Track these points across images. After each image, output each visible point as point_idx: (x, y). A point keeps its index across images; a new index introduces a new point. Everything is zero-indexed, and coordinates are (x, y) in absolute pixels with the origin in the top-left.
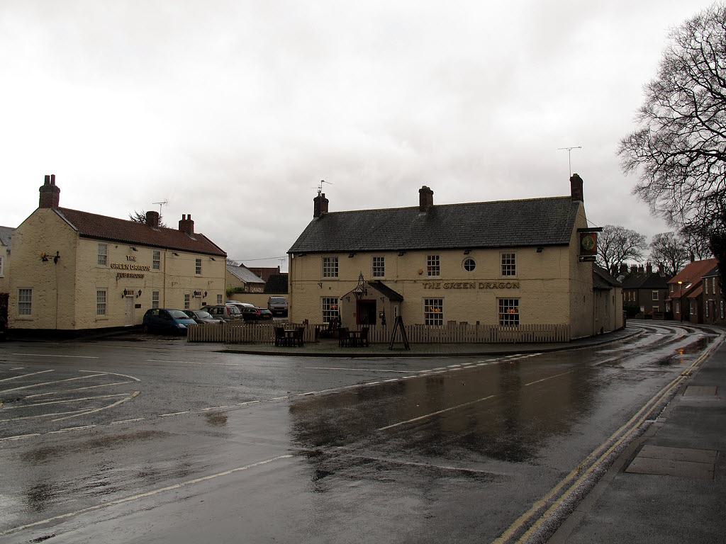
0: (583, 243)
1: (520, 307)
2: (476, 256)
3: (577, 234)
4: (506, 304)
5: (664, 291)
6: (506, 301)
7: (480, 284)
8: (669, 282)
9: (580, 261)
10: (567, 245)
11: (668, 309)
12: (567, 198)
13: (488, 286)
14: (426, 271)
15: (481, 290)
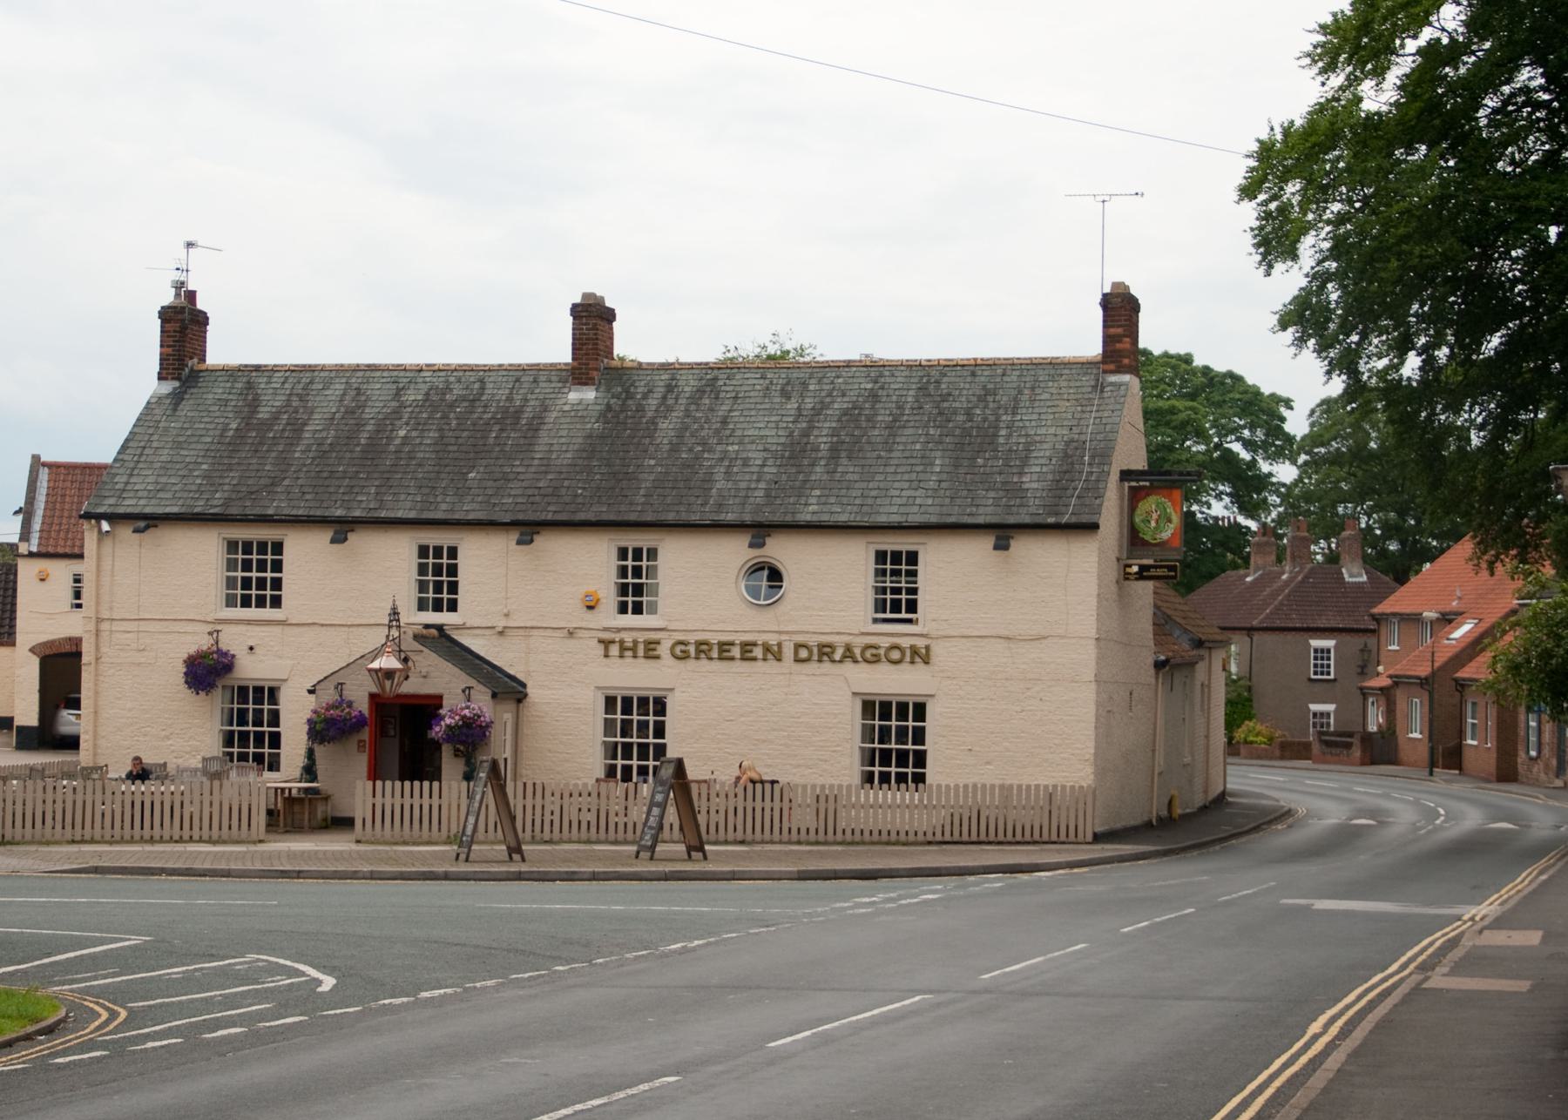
0: (1137, 520)
1: (931, 725)
2: (780, 550)
3: (1121, 489)
4: (885, 716)
5: (1357, 642)
6: (627, 701)
7: (798, 646)
8: (1385, 608)
9: (1127, 576)
10: (1094, 527)
11: (1375, 720)
12: (1085, 365)
13: (825, 652)
14: (610, 598)
15: (799, 666)
